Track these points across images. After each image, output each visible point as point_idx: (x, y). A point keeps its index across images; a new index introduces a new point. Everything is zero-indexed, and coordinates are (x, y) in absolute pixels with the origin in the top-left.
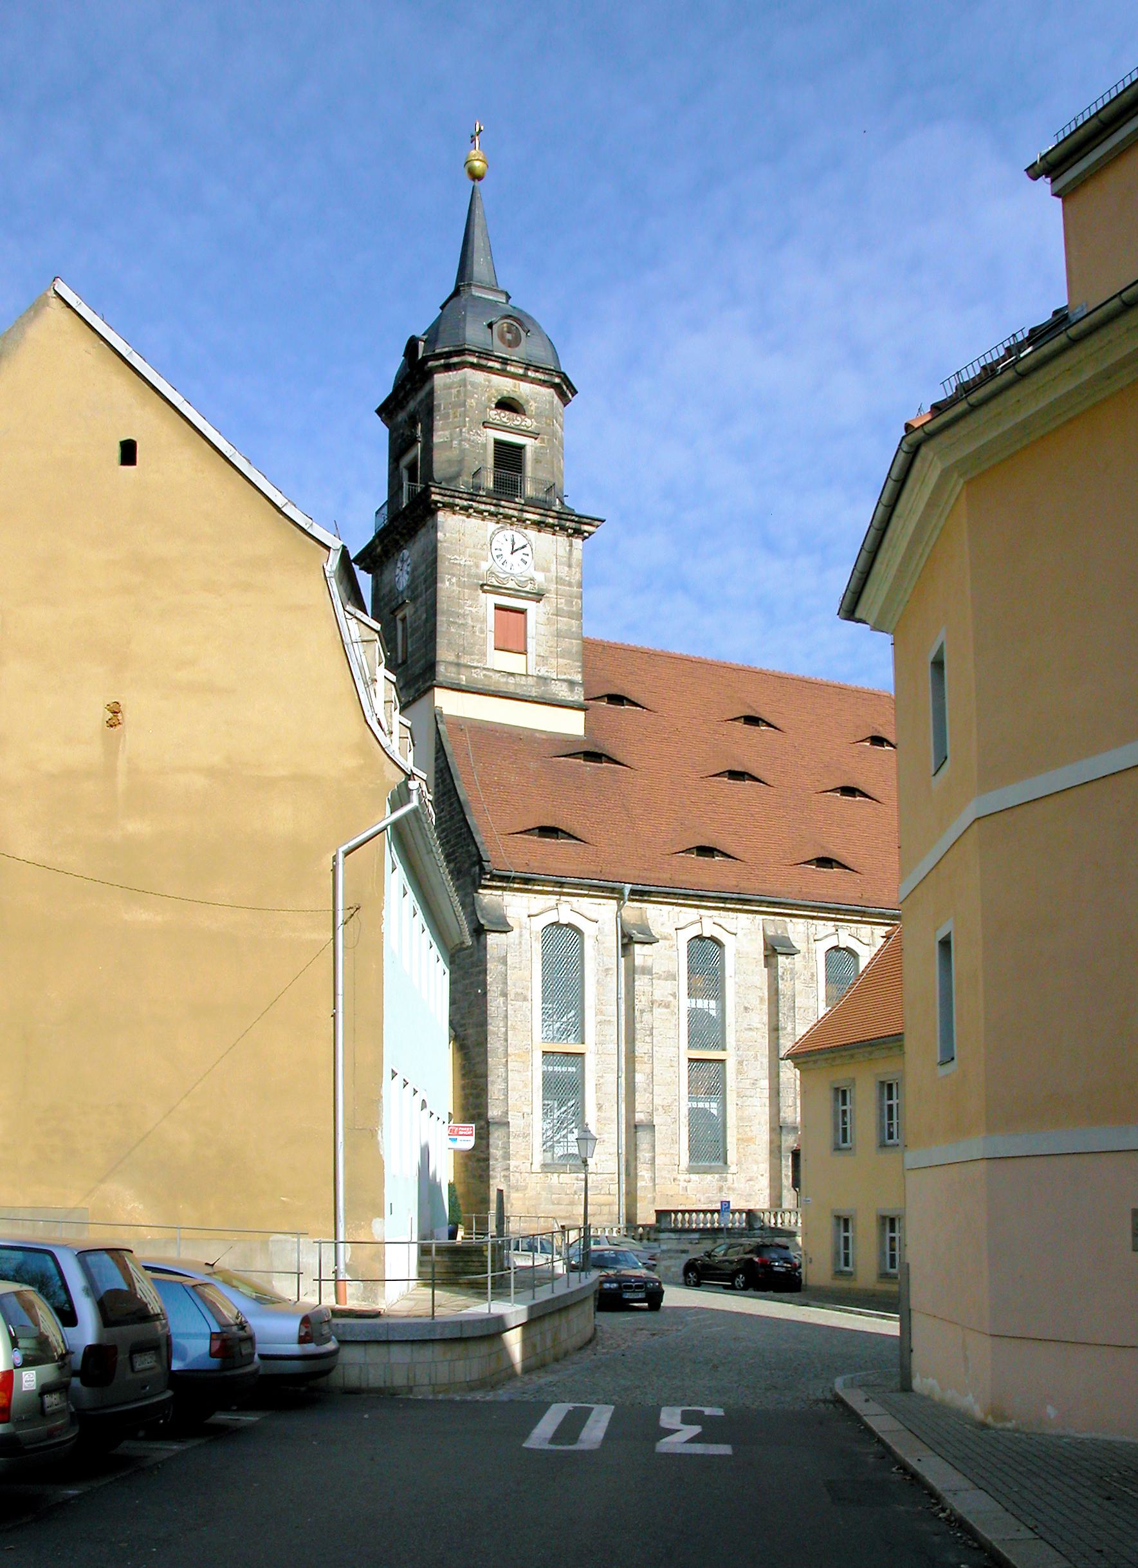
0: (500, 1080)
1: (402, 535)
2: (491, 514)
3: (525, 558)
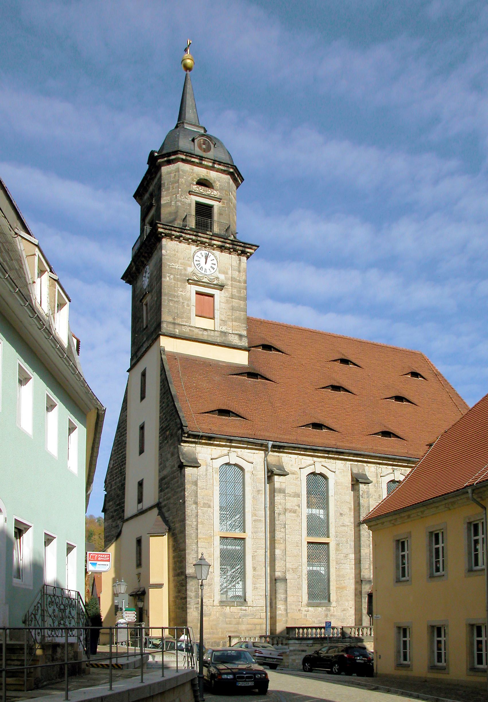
0: (193, 552)
1: (144, 257)
2: (193, 241)
3: (213, 266)
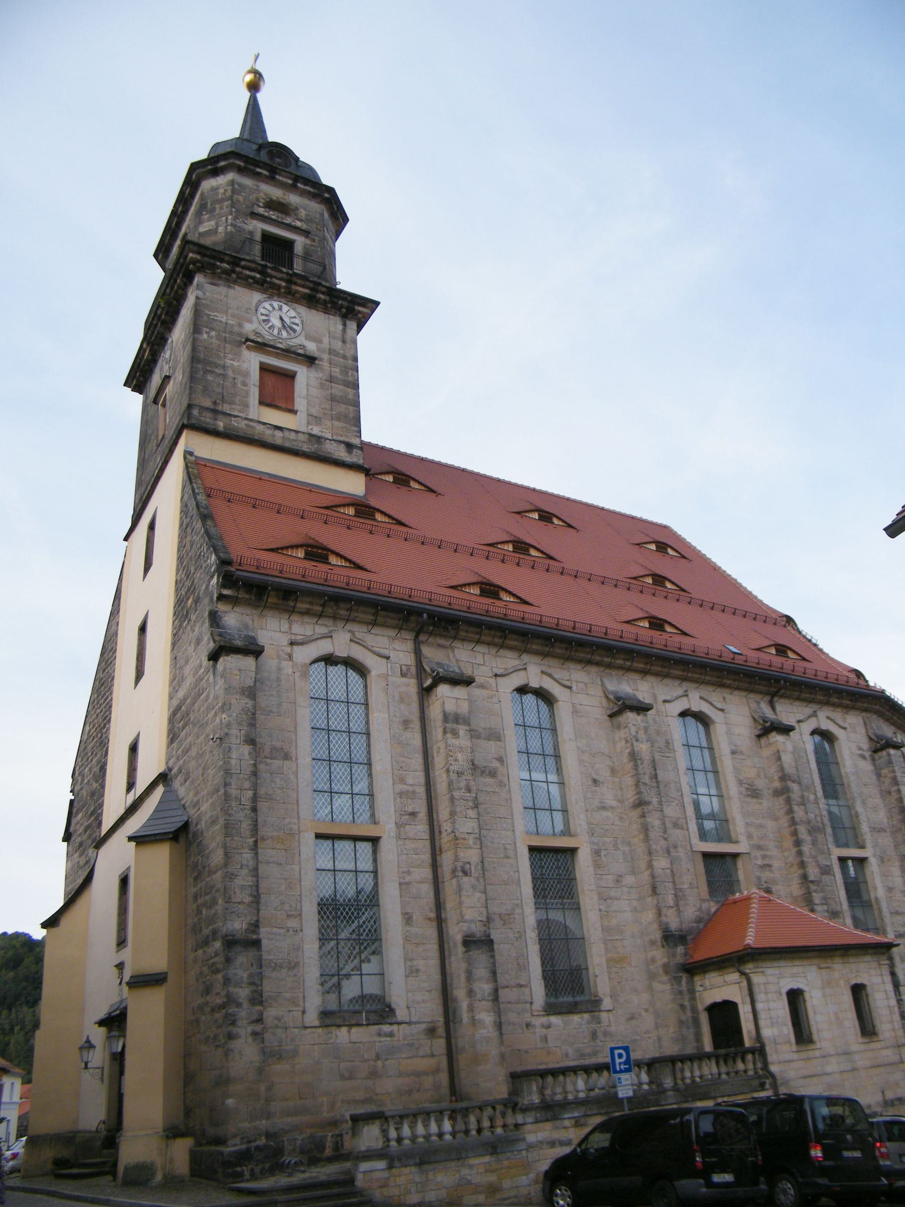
2: (256, 281)
